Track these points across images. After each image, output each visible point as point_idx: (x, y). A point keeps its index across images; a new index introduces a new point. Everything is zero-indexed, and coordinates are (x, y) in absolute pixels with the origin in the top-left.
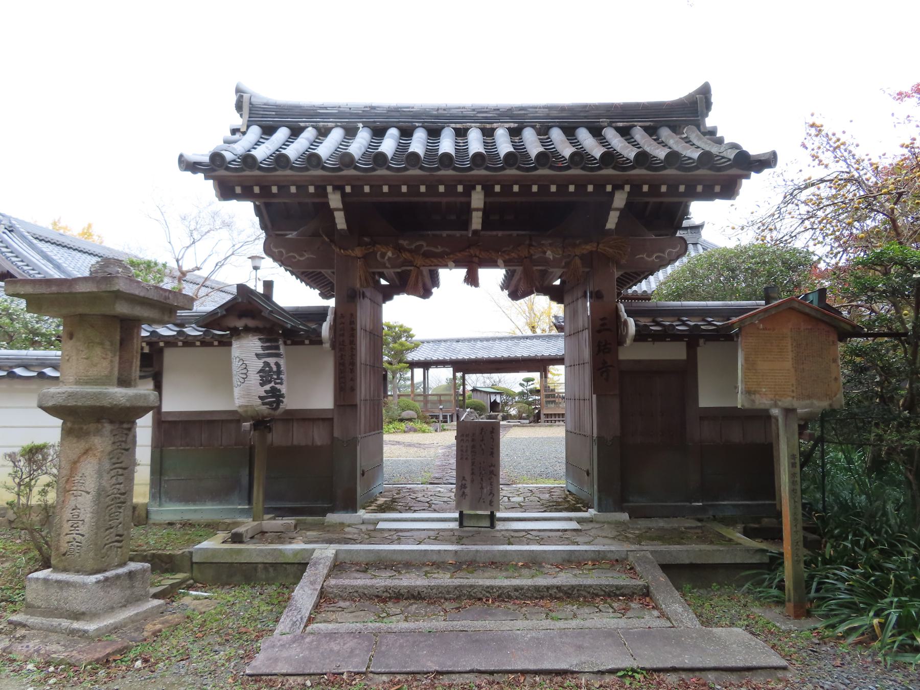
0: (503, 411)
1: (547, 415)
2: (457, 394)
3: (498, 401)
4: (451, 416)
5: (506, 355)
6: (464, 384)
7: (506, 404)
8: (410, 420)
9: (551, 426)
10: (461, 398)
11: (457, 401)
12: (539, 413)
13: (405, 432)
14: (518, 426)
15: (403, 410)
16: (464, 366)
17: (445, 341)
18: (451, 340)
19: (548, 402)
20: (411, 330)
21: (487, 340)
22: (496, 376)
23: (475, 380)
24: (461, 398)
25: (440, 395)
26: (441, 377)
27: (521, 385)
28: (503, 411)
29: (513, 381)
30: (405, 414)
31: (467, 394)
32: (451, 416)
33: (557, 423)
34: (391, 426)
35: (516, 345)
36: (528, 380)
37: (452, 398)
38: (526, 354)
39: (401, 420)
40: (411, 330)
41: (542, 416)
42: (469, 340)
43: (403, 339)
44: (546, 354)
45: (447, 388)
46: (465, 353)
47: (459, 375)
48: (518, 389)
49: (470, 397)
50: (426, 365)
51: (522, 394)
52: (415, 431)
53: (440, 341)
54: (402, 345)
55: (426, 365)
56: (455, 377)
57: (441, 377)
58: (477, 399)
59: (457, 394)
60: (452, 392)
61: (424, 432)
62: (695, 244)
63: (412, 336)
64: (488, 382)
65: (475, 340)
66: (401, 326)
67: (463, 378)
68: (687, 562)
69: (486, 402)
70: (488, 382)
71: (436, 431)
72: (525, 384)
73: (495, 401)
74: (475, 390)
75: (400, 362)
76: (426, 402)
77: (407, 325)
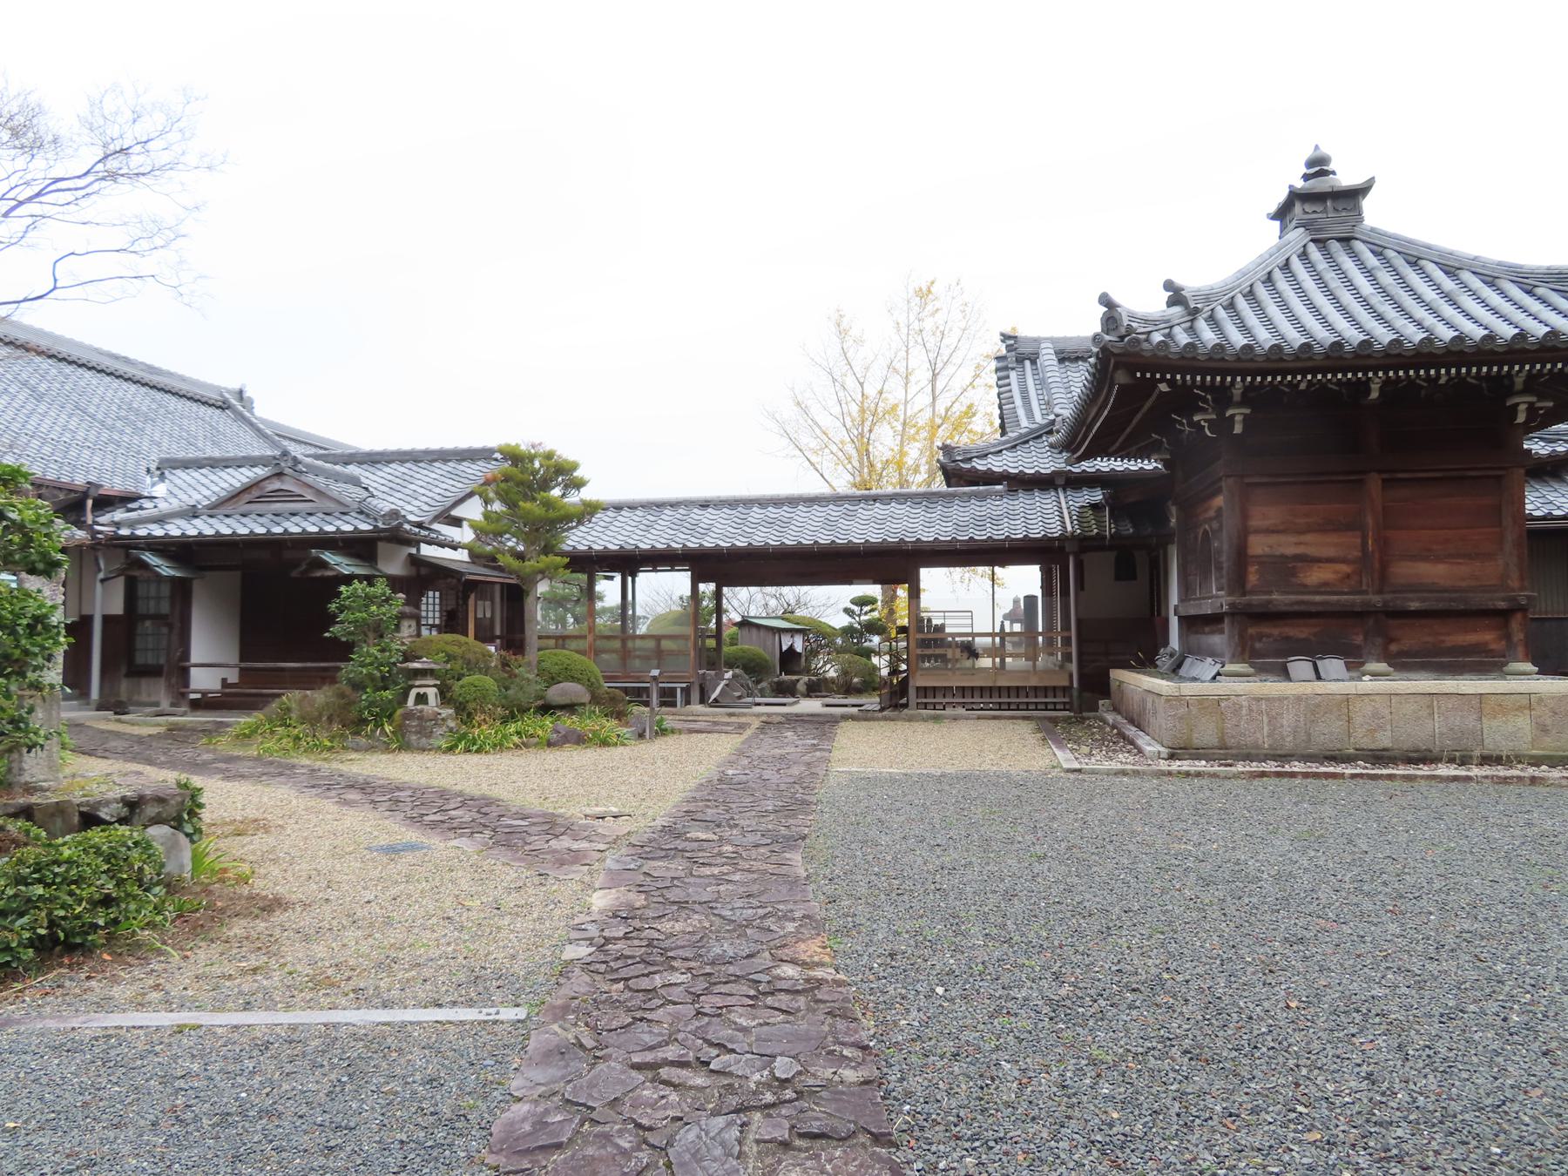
0: (808, 671)
1: (923, 691)
2: (701, 635)
3: (799, 648)
4: (687, 692)
5: (824, 539)
6: (719, 610)
7: (813, 653)
8: (570, 708)
9: (936, 719)
10: (711, 643)
11: (701, 651)
12: (904, 684)
13: (550, 744)
14: (853, 718)
15: (553, 680)
16: (717, 567)
17: (674, 505)
18: (688, 504)
19: (923, 658)
20: (575, 466)
21: (777, 502)
22: (790, 593)
23: (744, 601)
24: (711, 643)
25: (658, 639)
26: (662, 593)
27: (847, 611)
28: (808, 671)
29: (831, 604)
30: (555, 694)
31: (727, 632)
32: (687, 692)
33: (949, 711)
34: (512, 728)
35: (849, 516)
36: (862, 602)
37: (690, 644)
38: (875, 537)
39: (546, 709)
40: (575, 466)
41: (912, 692)
42: (732, 503)
43: (556, 492)
44: (927, 537)
45: (678, 620)
46: (720, 534)
47: (707, 588)
48: (840, 621)
49: (734, 641)
50: (628, 563)
51: (848, 631)
52: (580, 740)
53: (660, 505)
54: (548, 504)
55: (628, 563)
56: (695, 595)
57: (662, 593)
58: (750, 645)
59: (701, 635)
60: (688, 630)
61: (605, 743)
62: (1346, 241)
63: (579, 484)
64: (773, 603)
65: (748, 503)
66: (549, 456)
67: (718, 595)
68: (916, 724)
69: (769, 652)
70: (773, 603)
71: (641, 736)
72: (857, 609)
73: (791, 649)
74: (745, 624)
75: (547, 550)
76: (625, 654)
77: (566, 452)
